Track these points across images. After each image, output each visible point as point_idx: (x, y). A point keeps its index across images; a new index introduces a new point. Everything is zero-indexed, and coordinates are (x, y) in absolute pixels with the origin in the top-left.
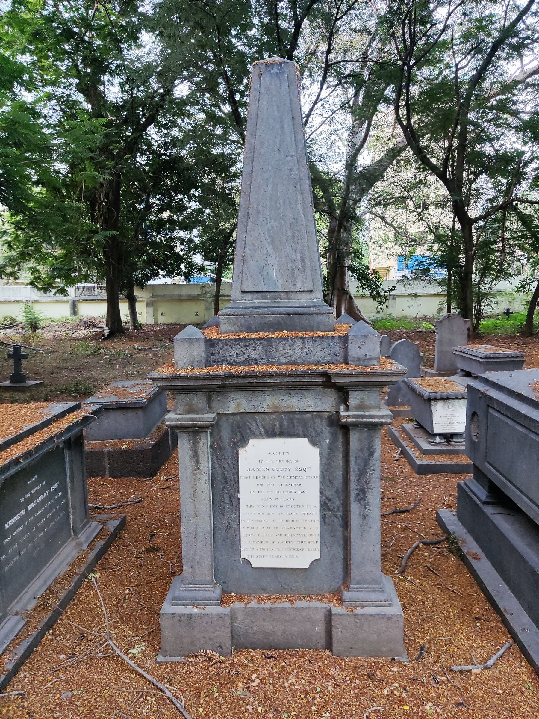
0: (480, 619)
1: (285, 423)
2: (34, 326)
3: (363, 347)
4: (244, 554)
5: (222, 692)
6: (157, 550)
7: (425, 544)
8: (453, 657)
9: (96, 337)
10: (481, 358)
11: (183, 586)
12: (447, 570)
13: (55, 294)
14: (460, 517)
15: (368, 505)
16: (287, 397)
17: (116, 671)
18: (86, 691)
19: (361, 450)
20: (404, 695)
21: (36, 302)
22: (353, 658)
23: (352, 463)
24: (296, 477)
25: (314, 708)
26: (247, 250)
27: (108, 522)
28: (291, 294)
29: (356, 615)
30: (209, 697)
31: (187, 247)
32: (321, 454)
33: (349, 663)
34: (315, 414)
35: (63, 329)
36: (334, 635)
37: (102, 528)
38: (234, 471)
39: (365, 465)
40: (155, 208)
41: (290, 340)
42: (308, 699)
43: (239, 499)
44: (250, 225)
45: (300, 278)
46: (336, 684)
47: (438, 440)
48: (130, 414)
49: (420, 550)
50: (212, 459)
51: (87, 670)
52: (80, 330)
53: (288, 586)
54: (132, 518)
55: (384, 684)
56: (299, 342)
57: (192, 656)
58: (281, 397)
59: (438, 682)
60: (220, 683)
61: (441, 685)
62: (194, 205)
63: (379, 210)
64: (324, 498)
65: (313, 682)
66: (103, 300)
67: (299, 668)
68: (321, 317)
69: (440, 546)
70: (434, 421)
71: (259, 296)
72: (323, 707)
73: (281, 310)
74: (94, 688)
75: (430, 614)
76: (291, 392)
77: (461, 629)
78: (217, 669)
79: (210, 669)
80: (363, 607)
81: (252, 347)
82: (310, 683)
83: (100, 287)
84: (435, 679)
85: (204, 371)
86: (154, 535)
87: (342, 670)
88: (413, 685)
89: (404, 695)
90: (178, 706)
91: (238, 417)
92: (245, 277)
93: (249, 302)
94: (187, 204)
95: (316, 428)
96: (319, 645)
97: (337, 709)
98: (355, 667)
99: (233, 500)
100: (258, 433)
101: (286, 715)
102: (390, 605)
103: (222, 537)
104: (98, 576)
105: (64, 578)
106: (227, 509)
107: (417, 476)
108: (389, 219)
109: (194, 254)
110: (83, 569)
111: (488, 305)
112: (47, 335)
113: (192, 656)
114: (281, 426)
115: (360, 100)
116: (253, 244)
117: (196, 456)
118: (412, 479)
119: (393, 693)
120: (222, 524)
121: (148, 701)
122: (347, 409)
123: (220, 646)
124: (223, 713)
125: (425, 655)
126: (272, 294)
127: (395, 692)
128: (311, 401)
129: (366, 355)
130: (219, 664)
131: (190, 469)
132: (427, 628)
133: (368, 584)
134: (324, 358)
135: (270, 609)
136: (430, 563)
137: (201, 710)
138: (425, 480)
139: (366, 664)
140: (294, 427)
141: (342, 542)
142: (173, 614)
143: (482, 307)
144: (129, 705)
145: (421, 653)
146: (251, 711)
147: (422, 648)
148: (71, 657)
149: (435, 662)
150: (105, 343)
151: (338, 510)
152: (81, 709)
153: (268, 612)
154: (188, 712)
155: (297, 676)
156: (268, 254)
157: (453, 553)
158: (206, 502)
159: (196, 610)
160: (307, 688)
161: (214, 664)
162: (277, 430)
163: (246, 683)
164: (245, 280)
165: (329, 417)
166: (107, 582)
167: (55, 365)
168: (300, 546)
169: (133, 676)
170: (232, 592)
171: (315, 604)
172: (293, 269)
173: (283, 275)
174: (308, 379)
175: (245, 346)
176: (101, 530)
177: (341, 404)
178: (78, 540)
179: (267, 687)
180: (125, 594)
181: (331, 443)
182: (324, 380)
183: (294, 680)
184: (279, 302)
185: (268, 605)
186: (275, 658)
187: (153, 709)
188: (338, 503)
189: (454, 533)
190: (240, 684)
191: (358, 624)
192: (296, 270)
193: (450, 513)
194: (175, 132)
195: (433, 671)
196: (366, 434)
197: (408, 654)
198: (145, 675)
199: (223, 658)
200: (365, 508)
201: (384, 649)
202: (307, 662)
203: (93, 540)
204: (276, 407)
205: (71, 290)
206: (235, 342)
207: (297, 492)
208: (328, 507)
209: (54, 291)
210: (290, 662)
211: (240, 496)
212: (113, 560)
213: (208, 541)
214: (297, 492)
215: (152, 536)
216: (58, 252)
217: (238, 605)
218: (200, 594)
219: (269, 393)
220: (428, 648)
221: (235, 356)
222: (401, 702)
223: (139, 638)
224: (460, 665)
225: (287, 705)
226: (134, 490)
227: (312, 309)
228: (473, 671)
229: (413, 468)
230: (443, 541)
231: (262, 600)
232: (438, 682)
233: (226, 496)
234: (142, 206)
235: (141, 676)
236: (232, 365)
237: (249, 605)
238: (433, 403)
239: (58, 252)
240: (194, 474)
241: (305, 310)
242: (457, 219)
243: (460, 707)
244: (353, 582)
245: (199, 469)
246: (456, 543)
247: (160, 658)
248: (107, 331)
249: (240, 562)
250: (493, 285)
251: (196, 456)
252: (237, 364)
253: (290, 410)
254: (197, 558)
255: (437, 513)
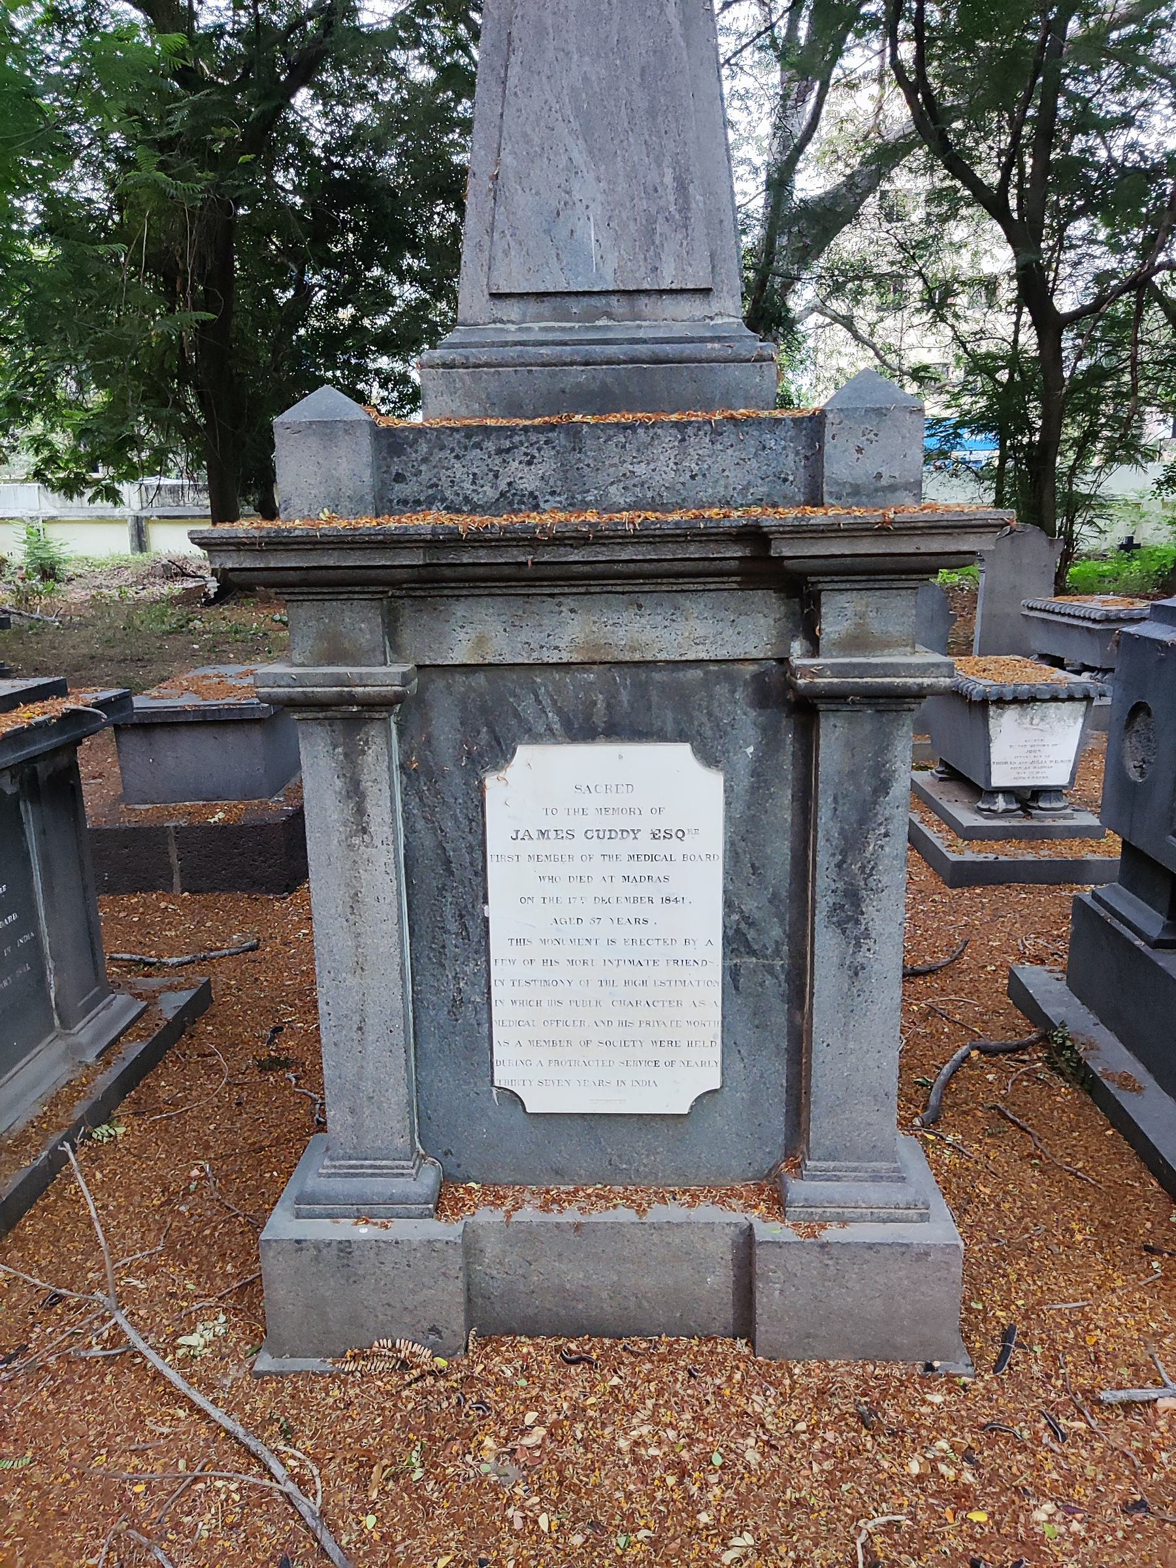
0: (1160, 1253)
1: (624, 697)
2: (48, 571)
3: (869, 450)
4: (502, 1076)
5: (435, 1465)
6: (286, 1064)
7: (983, 1051)
8: (1097, 1360)
9: (188, 597)
10: (1095, 621)
11: (327, 1162)
12: (1052, 1119)
13: (92, 500)
14: (1078, 984)
15: (868, 937)
16: (628, 615)
17: (136, 1400)
18: (42, 1459)
19: (852, 774)
20: (968, 1477)
21: (51, 520)
22: (814, 1364)
23: (824, 815)
24: (653, 858)
25: (704, 1518)
26: (508, 159)
27: (162, 996)
28: (643, 300)
29: (823, 1246)
30: (396, 1481)
31: (396, 394)
32: (728, 790)
33: (803, 1380)
34: (713, 668)
35: (115, 582)
36: (761, 1300)
37: (144, 1010)
38: (470, 838)
39: (862, 822)
40: (320, 296)
41: (640, 431)
42: (686, 1490)
43: (486, 920)
44: (514, 71)
45: (671, 247)
46: (767, 1443)
47: (1001, 803)
48: (232, 738)
49: (972, 1066)
50: (405, 804)
51: (52, 1394)
52: (153, 584)
53: (629, 1162)
54: (229, 987)
55: (909, 1444)
56: (669, 438)
57: (354, 1357)
58: (611, 617)
59: (1064, 1437)
60: (431, 1438)
61: (1073, 1445)
62: (407, 293)
63: (839, 306)
64: (735, 917)
65: (702, 1435)
66: (206, 517)
67: (659, 1393)
68: (735, 372)
69: (1026, 1057)
70: (995, 757)
71: (546, 307)
72: (731, 1514)
73: (611, 350)
74: (64, 1452)
75: (1020, 1237)
76: (642, 599)
77: (1109, 1278)
78: (424, 1393)
79: (405, 1393)
80: (844, 1222)
81: (519, 454)
82: (692, 1440)
83: (197, 490)
84: (1053, 1427)
85: (367, 523)
86: (281, 1029)
87: (785, 1399)
88: (991, 1445)
89: (968, 1477)
90: (304, 1509)
91: (480, 679)
92: (500, 245)
93: (512, 327)
94: (396, 291)
95: (717, 712)
96: (716, 1327)
97: (772, 1521)
98: (822, 1392)
99: (470, 924)
100: (541, 729)
101: (622, 1540)
102: (924, 1218)
103: (440, 1027)
104: (121, 1130)
105: (23, 1139)
106: (451, 950)
107: (949, 890)
108: (863, 329)
109: (412, 411)
110: (77, 1114)
111: (1091, 523)
112: (76, 594)
113: (354, 1357)
114: (609, 706)
115: (803, 27)
116: (525, 135)
117: (355, 792)
118: (937, 898)
119: (935, 1469)
120: (438, 992)
121: (218, 1492)
122: (814, 647)
123: (434, 1330)
124: (435, 1531)
125: (1017, 1354)
126: (585, 301)
127: (943, 1468)
128: (702, 629)
129: (879, 476)
130: (430, 1380)
131: (338, 833)
132: (1014, 1277)
133: (859, 1159)
134: (745, 488)
135: (578, 1227)
136: (1004, 1098)
137: (370, 1521)
138: (971, 899)
139: (852, 1382)
140: (649, 708)
141: (785, 1044)
142: (298, 1242)
143: (1076, 528)
144: (161, 1503)
145: (1006, 1351)
146: (518, 1524)
147: (1007, 1335)
148: (15, 1356)
149: (1049, 1377)
150: (210, 610)
151: (777, 952)
152: (17, 1516)
153: (571, 1236)
154: (334, 1529)
155: (654, 1419)
156: (573, 170)
157: (1062, 1074)
158: (390, 926)
159: (364, 1230)
160: (685, 1455)
161: (417, 1380)
162: (600, 717)
163: (507, 1439)
164: (500, 254)
165: (758, 677)
166: (143, 1147)
167: (85, 651)
168: (663, 1054)
169: (182, 1414)
170: (469, 1179)
171: (706, 1212)
172: (651, 220)
173: (617, 238)
174: (694, 552)
175: (499, 452)
176: (139, 1016)
177: (794, 637)
178: (71, 1040)
179: (568, 1451)
180: (190, 1179)
181: (759, 759)
182: (747, 552)
183: (645, 1430)
184: (606, 328)
185: (571, 1215)
186: (590, 1362)
187: (229, 1519)
188: (776, 932)
189: (1063, 1025)
190: (489, 1442)
191: (831, 1271)
192: (661, 219)
193: (1046, 975)
194: (360, 113)
195: (1047, 1402)
196: (868, 727)
197: (970, 1350)
198: (216, 1413)
199: (442, 1363)
200: (858, 945)
201: (902, 1340)
202: (681, 1375)
203: (115, 1041)
204: (597, 647)
205: (127, 490)
206: (468, 436)
207: (657, 901)
208: (747, 944)
209: (89, 493)
210: (634, 1374)
211: (492, 910)
212: (165, 1089)
213: (399, 1038)
214: (657, 901)
215: (277, 1030)
216: (96, 398)
217: (487, 1216)
218: (377, 1186)
219: (573, 605)
220: (1025, 1335)
221: (467, 485)
222: (962, 1498)
223: (212, 1301)
224: (1120, 1387)
225: (625, 1507)
226: (241, 922)
227: (709, 346)
228: (1162, 1404)
229: (938, 871)
230: (1032, 1043)
231: (554, 1201)
232: (1064, 1437)
233: (449, 911)
234: (290, 293)
235: (204, 1415)
236: (459, 511)
237: (517, 1216)
238: (992, 710)
239: (96, 398)
240: (351, 847)
241: (688, 349)
242: (1026, 318)
243: (1138, 1516)
244: (816, 1153)
245: (364, 831)
246: (1071, 1048)
247: (265, 1363)
248: (213, 586)
249: (490, 1098)
250: (1103, 476)
251: (355, 792)
252: (475, 509)
253: (637, 657)
254: (368, 1086)
255: (1012, 976)
